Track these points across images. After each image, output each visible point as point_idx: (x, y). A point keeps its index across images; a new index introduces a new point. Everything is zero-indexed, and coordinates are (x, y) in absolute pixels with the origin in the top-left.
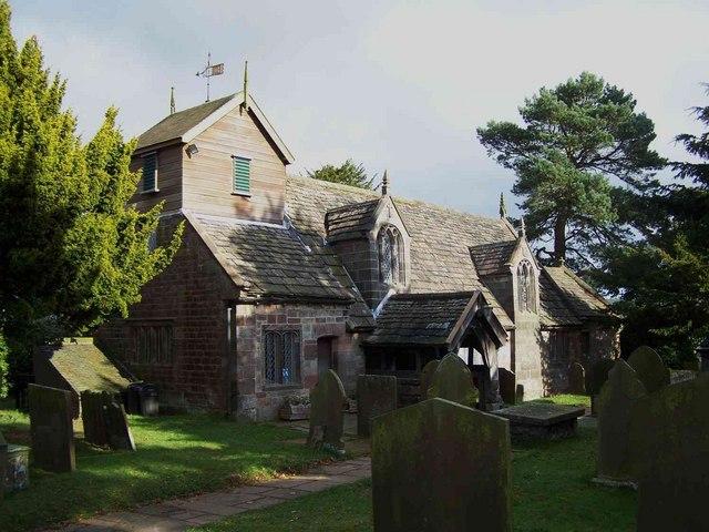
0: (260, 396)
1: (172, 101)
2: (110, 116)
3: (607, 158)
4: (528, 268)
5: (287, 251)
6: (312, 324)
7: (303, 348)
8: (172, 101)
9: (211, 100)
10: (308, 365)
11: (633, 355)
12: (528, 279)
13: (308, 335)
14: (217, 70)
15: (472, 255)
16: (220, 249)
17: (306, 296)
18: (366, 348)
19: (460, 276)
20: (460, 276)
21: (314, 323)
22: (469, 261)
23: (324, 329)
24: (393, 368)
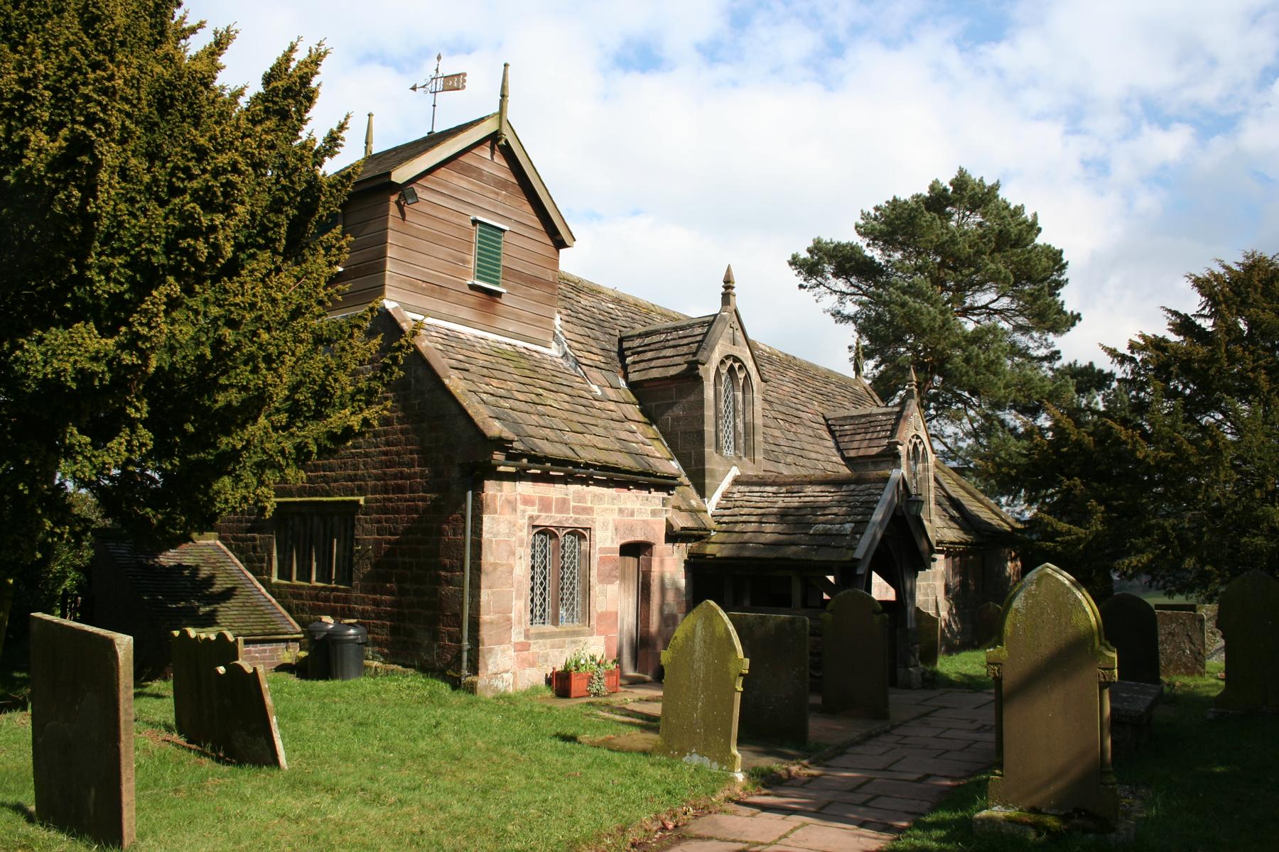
0: (522, 647)
1: (504, 88)
2: (348, 116)
3: (986, 307)
4: (921, 448)
5: (653, 364)
6: (613, 517)
7: (594, 562)
8: (504, 88)
9: (437, 130)
10: (604, 593)
11: (920, 679)
12: (920, 466)
13: (605, 540)
14: (454, 82)
15: (828, 426)
16: (454, 374)
17: (605, 468)
18: (695, 565)
19: (820, 457)
20: (820, 457)
21: (616, 516)
22: (826, 435)
23: (631, 529)
24: (747, 603)
